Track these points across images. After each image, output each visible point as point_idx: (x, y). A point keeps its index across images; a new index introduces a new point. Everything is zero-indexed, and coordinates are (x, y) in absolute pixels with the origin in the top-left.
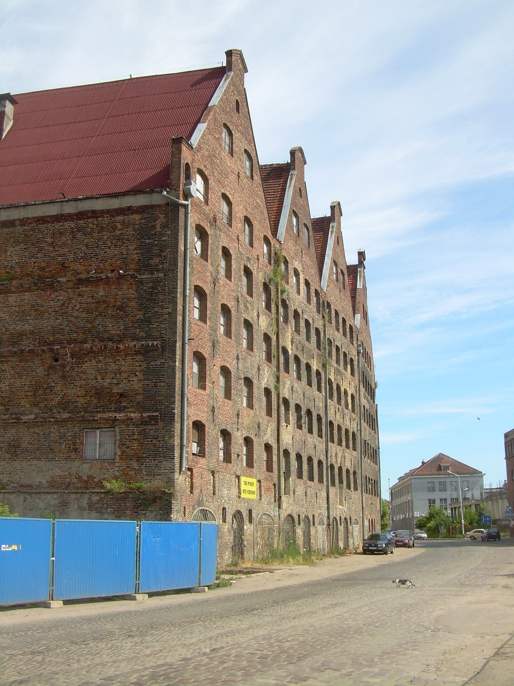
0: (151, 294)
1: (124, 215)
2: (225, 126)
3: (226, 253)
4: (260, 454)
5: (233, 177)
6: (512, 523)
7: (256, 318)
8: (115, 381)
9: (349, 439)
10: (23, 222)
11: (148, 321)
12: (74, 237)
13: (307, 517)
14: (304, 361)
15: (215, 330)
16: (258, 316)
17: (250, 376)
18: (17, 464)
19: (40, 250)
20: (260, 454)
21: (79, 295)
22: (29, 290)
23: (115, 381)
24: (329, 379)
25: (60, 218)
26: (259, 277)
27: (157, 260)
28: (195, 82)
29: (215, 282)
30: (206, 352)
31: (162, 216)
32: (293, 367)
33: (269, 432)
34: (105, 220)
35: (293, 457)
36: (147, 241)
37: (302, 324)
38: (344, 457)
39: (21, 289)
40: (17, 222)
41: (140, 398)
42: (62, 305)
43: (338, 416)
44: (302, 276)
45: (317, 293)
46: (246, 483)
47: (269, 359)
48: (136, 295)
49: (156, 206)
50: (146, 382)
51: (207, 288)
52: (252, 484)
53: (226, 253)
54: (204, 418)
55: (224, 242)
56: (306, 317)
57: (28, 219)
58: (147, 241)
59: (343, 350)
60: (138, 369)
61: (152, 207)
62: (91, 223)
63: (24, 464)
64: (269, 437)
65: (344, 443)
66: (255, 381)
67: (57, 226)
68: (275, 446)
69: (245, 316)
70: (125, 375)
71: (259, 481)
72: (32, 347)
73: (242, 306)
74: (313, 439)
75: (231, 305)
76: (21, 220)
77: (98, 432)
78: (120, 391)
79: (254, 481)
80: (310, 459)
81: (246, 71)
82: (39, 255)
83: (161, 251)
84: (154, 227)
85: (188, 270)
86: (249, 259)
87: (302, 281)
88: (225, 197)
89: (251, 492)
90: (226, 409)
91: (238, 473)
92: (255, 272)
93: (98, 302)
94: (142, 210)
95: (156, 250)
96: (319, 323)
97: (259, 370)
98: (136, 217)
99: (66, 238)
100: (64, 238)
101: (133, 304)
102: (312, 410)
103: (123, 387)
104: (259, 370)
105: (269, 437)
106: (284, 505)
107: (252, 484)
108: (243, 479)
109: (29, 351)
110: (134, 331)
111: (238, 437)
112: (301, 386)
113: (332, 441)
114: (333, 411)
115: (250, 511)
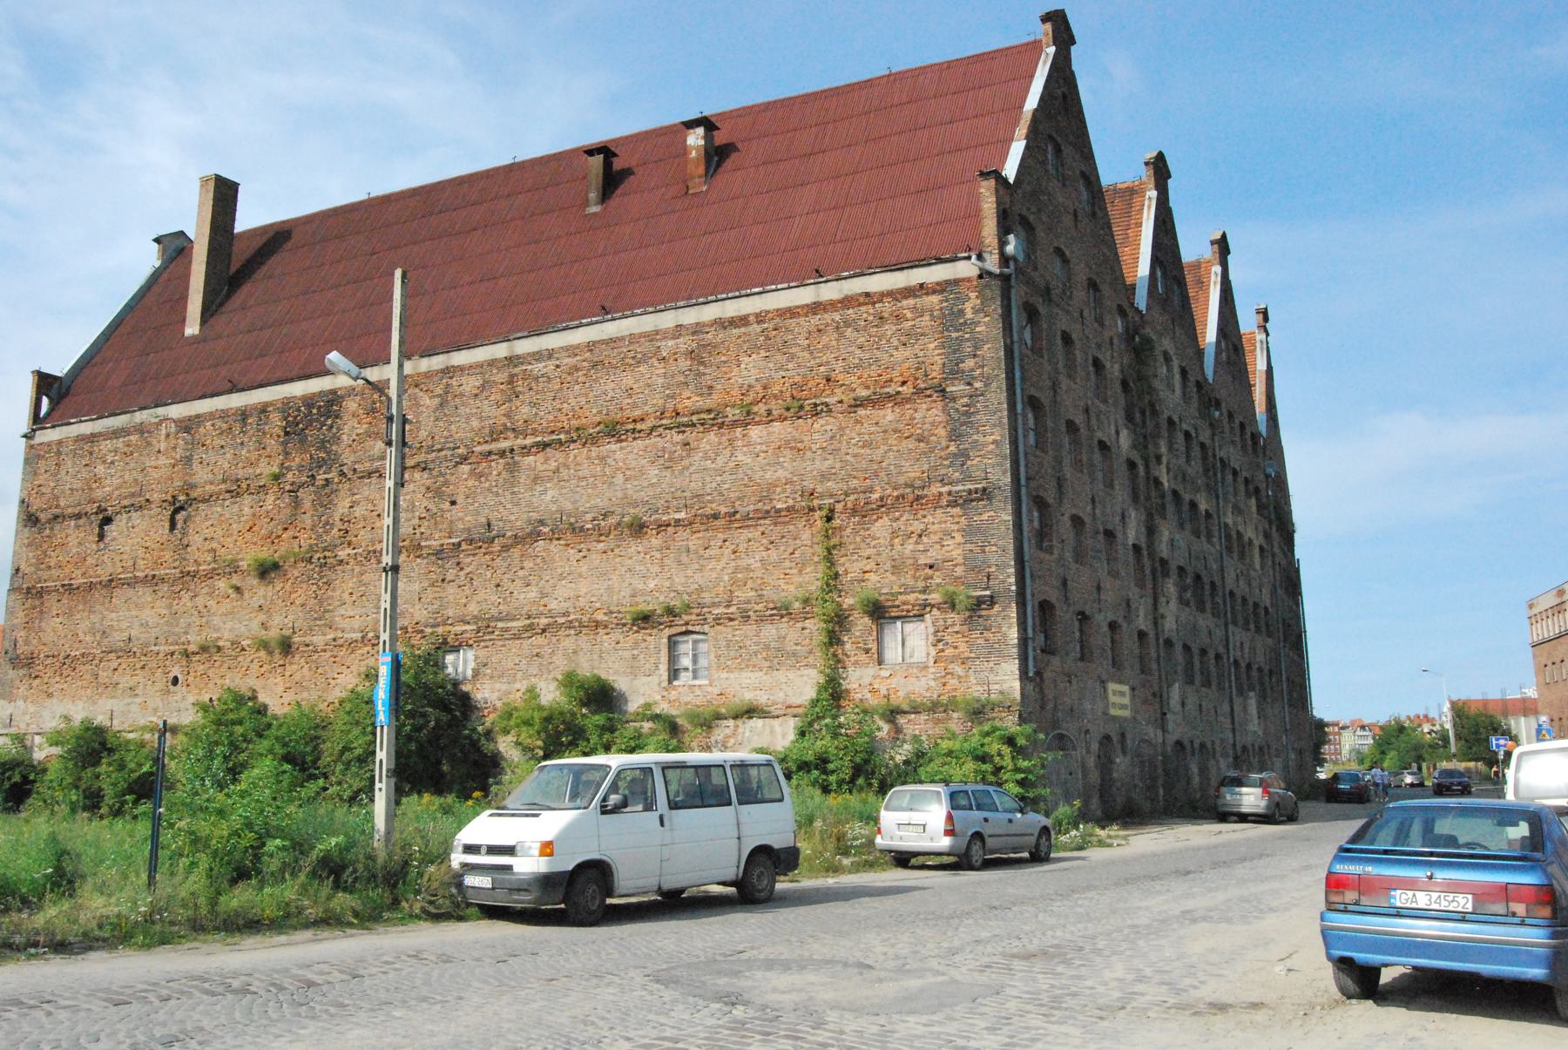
0: (966, 413)
1: (916, 296)
2: (1050, 137)
3: (1067, 339)
4: (1129, 644)
5: (1068, 220)
6: (992, 1041)
7: (1114, 436)
8: (921, 547)
9: (1256, 617)
10: (760, 317)
11: (964, 455)
12: (842, 335)
13: (1203, 746)
14: (1187, 497)
15: (1058, 460)
16: (1117, 433)
17: (1110, 527)
18: (781, 675)
19: (793, 357)
20: (1129, 644)
21: (857, 422)
22: (782, 419)
23: (921, 547)
24: (1226, 525)
25: (816, 308)
26: (1114, 370)
27: (970, 363)
28: (1169, 211)
29: (1055, 387)
30: (1050, 497)
31: (973, 295)
32: (1170, 508)
33: (1142, 613)
34: (886, 307)
35: (1178, 648)
36: (954, 335)
37: (1180, 437)
38: (1248, 645)
39: (770, 417)
40: (751, 318)
41: (959, 571)
42: (832, 438)
43: (1241, 583)
44: (1176, 363)
45: (1199, 385)
46: (1115, 693)
47: (1135, 498)
48: (942, 418)
49: (963, 280)
50: (969, 546)
51: (1045, 398)
52: (1122, 694)
53: (1067, 339)
54: (1053, 596)
55: (1063, 323)
56: (1185, 426)
57: (767, 312)
58: (954, 335)
59: (1244, 474)
60: (956, 527)
61: (956, 282)
62: (867, 311)
63: (791, 675)
64: (1142, 622)
65: (1252, 626)
66: (1119, 535)
67: (814, 320)
68: (1152, 635)
69: (1099, 434)
70: (935, 538)
71: (1133, 689)
72: (791, 502)
73: (1094, 421)
74: (1205, 621)
75: (1079, 419)
76: (757, 315)
77: (899, 624)
78: (929, 561)
79: (1125, 688)
80: (1203, 652)
81: (1074, 43)
82: (790, 366)
83: (976, 348)
84: (962, 312)
85: (1018, 374)
86: (1099, 346)
87: (1176, 370)
88: (1059, 251)
89: (1123, 707)
90: (1082, 581)
91: (1105, 677)
92: (1108, 365)
93: (885, 432)
94: (942, 287)
95: (968, 348)
96: (1205, 436)
97: (1123, 517)
98: (935, 299)
99: (829, 338)
100: (825, 339)
101: (941, 432)
102: (1203, 574)
103: (934, 555)
104: (1123, 517)
105: (1142, 622)
106: (1170, 726)
107: (1122, 694)
108: (1112, 686)
109: (788, 509)
110: (943, 472)
111: (1101, 620)
112: (1182, 539)
113: (1235, 623)
114: (1233, 575)
115: (1123, 735)
